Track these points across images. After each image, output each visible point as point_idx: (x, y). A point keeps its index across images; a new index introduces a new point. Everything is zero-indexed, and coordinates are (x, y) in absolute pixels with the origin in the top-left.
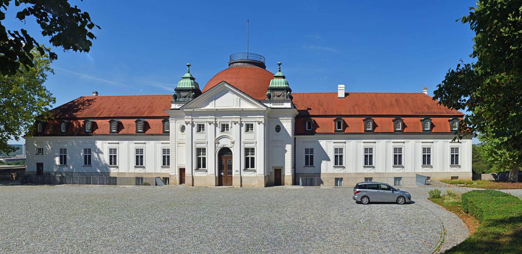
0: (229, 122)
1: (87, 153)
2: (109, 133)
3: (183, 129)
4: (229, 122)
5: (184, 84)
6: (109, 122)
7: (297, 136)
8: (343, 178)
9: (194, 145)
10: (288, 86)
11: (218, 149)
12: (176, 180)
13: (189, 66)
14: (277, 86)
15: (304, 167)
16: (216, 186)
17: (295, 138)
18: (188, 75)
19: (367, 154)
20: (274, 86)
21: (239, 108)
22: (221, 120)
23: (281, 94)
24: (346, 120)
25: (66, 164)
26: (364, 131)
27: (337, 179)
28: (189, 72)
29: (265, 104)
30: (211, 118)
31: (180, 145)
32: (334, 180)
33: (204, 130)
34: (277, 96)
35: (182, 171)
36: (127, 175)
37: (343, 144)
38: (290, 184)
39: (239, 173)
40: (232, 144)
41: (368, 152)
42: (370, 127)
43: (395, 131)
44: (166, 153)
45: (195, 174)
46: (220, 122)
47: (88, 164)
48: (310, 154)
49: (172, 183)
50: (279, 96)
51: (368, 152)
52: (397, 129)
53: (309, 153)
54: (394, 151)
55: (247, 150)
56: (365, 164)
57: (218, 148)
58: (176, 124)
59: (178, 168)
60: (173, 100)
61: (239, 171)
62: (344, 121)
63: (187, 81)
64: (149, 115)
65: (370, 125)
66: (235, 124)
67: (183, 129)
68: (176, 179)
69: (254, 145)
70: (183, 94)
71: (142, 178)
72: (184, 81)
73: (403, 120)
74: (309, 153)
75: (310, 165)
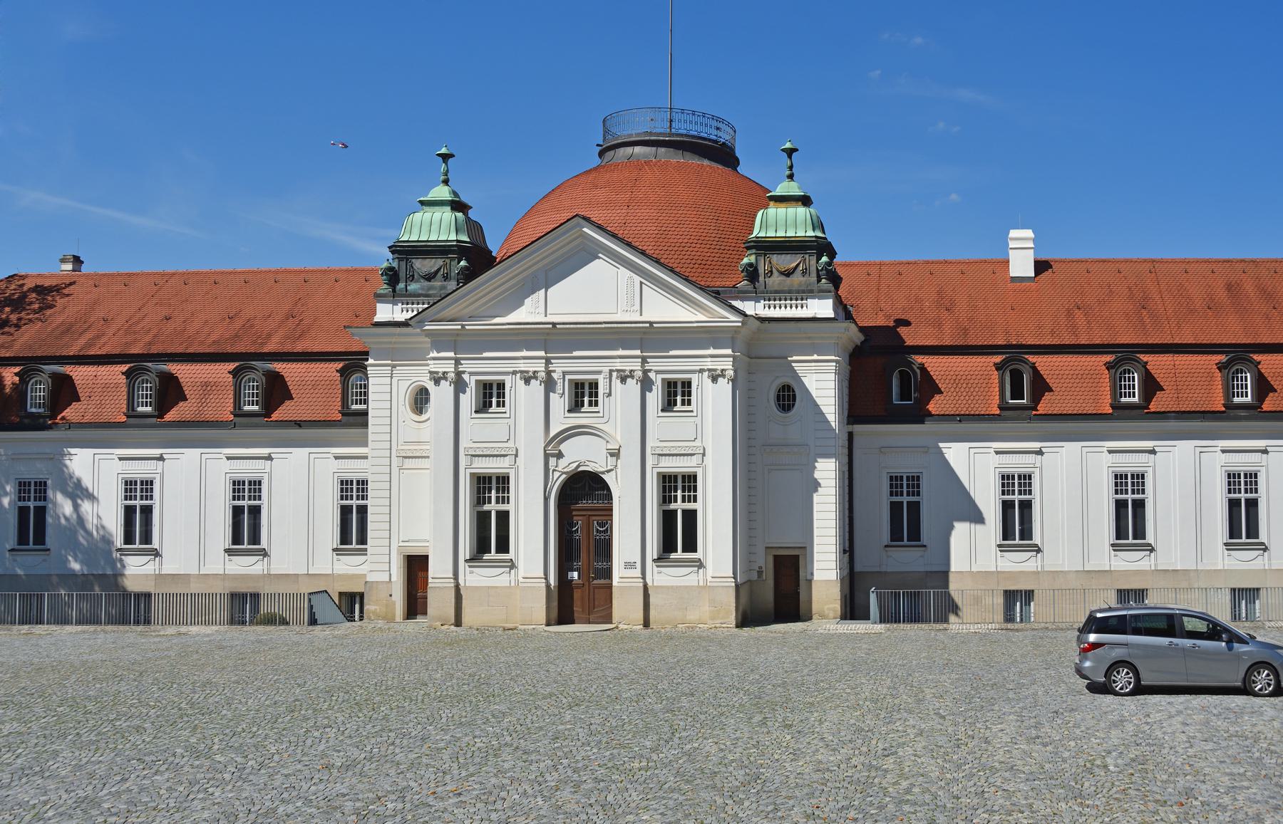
0: (599, 372)
1: (902, 495)
2: (124, 419)
3: (420, 400)
4: (599, 372)
5: (425, 229)
6: (123, 373)
7: (858, 429)
8: (1036, 592)
9: (650, 461)
10: (820, 234)
11: (558, 480)
12: (394, 603)
13: (445, 157)
14: (781, 234)
15: (886, 546)
16: (548, 624)
17: (851, 435)
18: (442, 192)
19: (1237, 496)
20: (771, 234)
21: (541, 319)
22: (569, 366)
23: (794, 265)
24: (1043, 363)
25: (44, 544)
26: (1113, 407)
27: (1010, 596)
28: (446, 182)
29: (737, 304)
30: (628, 360)
31: (409, 463)
32: (1000, 600)
33: (695, 501)
34: (782, 273)
35: (416, 566)
36: (192, 585)
37: (1144, 458)
38: (831, 615)
39: (637, 572)
40: (612, 461)
41: (1243, 487)
42: (1134, 393)
43: (1230, 406)
44: (905, 490)
45: (656, 577)
46: (564, 373)
47: (35, 544)
48: (1133, 493)
49: (374, 612)
50: (788, 274)
51: (1243, 487)
52: (1236, 400)
53: (354, 497)
54: (1229, 483)
55: (668, 483)
56: (20, 543)
57: (557, 474)
58: (395, 380)
59: (399, 552)
60: (384, 288)
61: (639, 565)
62: (1034, 368)
63: (437, 215)
64: (288, 348)
65: (1134, 385)
66: (623, 380)
67: (420, 400)
68: (394, 598)
69: (694, 461)
70: (423, 265)
71: (256, 597)
72: (428, 215)
73: (1259, 363)
74: (354, 497)
75: (34, 544)
